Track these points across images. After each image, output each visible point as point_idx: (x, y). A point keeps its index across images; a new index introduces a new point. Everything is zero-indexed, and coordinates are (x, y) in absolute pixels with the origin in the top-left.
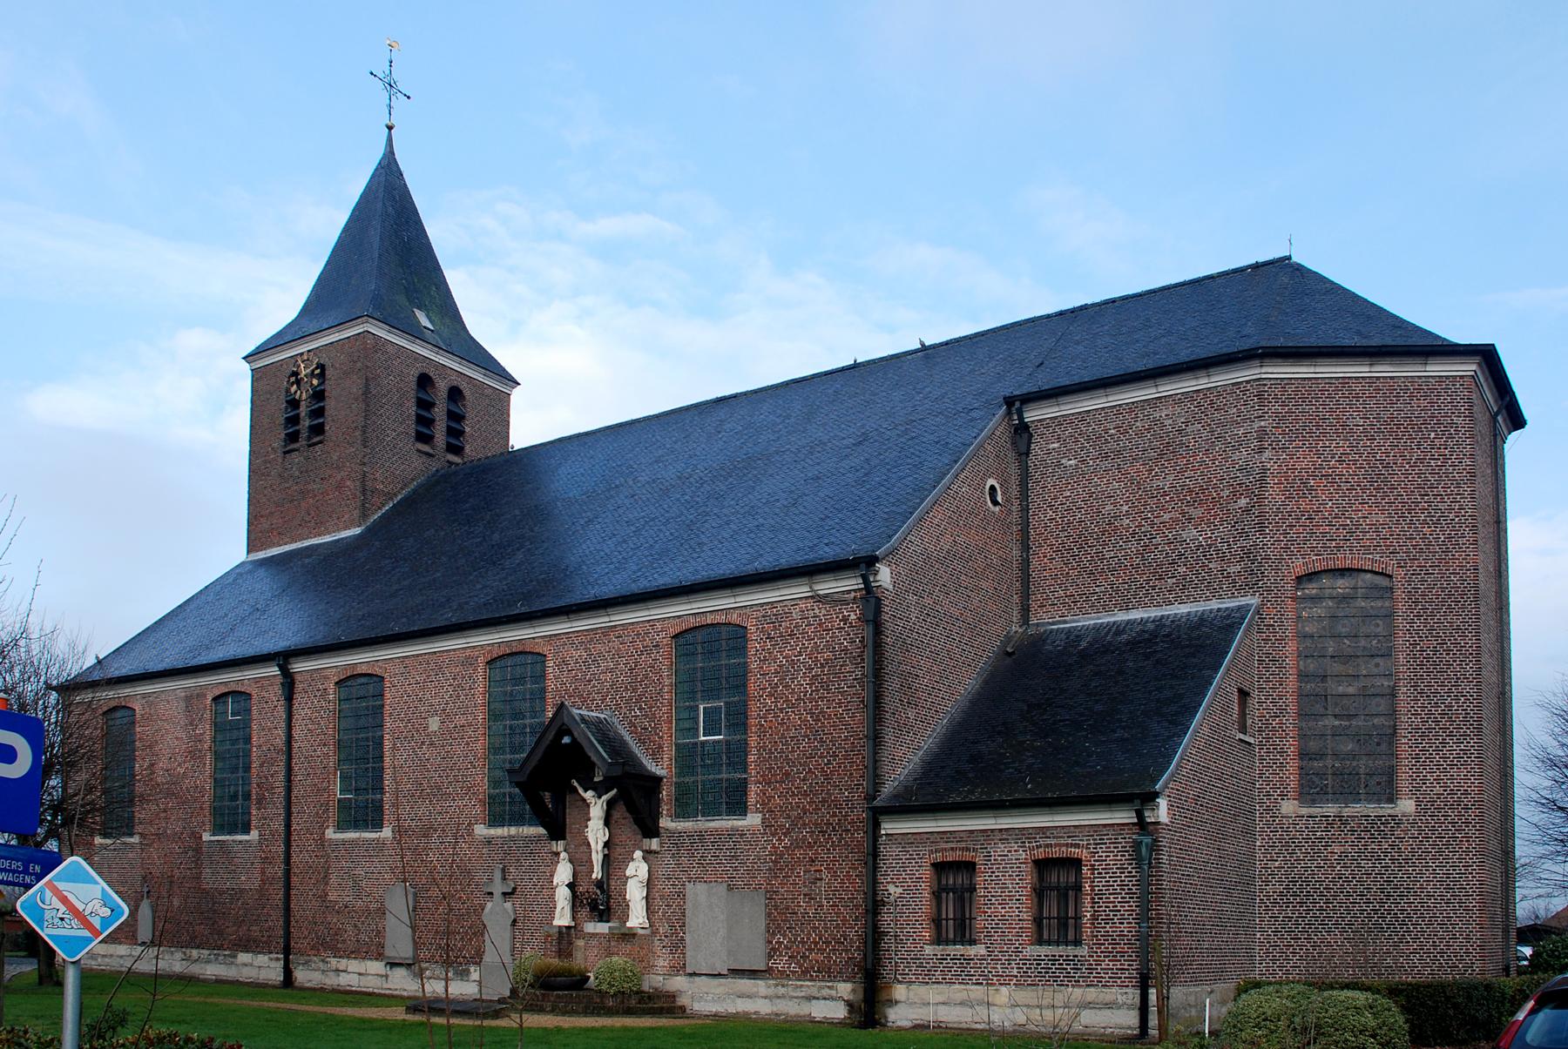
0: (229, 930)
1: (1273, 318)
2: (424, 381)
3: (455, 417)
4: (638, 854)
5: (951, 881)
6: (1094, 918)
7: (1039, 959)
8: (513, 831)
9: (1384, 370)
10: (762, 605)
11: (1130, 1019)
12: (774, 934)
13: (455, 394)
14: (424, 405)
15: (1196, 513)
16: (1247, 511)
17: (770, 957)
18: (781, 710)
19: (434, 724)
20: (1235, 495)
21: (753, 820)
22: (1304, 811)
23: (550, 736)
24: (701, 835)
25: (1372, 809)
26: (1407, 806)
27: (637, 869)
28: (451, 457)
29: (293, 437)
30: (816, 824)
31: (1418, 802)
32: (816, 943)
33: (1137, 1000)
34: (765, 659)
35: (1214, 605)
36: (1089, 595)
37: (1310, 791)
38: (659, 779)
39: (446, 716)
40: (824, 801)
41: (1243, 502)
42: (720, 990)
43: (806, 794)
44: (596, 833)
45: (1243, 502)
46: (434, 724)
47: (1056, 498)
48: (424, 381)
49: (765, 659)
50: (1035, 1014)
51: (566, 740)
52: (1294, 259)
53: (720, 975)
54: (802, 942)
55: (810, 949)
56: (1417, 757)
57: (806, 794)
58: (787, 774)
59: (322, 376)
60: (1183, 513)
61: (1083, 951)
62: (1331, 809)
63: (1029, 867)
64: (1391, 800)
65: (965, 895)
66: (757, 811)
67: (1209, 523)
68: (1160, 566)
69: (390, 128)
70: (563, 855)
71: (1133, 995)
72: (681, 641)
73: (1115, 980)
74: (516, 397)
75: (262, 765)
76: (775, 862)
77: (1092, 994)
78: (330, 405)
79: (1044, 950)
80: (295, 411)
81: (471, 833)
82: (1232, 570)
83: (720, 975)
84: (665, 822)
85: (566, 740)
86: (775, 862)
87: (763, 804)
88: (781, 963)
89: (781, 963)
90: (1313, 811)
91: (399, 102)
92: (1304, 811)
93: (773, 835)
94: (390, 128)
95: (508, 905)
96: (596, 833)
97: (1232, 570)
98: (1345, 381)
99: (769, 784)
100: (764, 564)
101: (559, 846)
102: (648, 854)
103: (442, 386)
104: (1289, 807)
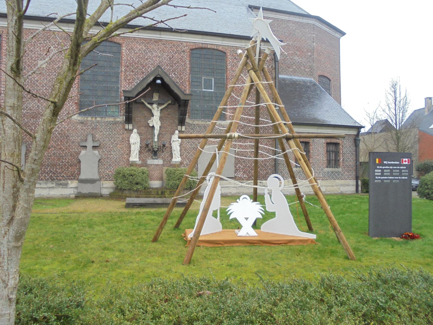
4: (177, 132)
5: (331, 149)
6: (343, 160)
7: (328, 172)
10: (233, 46)
11: (353, 189)
12: (237, 164)
15: (298, 53)
16: (310, 56)
17: (235, 172)
20: (308, 52)
23: (151, 79)
33: (355, 183)
34: (234, 66)
35: (303, 78)
41: (309, 54)
44: (155, 121)
45: (309, 54)
49: (234, 66)
50: (332, 188)
54: (249, 167)
60: (295, 53)
61: (340, 170)
63: (325, 145)
65: (337, 153)
67: (301, 57)
71: (354, 182)
73: (349, 178)
75: (290, 50)
77: (342, 182)
79: (330, 170)
82: (307, 70)
85: (159, 81)
89: (240, 175)
95: (96, 152)
96: (155, 121)
97: (307, 70)
101: (131, 127)
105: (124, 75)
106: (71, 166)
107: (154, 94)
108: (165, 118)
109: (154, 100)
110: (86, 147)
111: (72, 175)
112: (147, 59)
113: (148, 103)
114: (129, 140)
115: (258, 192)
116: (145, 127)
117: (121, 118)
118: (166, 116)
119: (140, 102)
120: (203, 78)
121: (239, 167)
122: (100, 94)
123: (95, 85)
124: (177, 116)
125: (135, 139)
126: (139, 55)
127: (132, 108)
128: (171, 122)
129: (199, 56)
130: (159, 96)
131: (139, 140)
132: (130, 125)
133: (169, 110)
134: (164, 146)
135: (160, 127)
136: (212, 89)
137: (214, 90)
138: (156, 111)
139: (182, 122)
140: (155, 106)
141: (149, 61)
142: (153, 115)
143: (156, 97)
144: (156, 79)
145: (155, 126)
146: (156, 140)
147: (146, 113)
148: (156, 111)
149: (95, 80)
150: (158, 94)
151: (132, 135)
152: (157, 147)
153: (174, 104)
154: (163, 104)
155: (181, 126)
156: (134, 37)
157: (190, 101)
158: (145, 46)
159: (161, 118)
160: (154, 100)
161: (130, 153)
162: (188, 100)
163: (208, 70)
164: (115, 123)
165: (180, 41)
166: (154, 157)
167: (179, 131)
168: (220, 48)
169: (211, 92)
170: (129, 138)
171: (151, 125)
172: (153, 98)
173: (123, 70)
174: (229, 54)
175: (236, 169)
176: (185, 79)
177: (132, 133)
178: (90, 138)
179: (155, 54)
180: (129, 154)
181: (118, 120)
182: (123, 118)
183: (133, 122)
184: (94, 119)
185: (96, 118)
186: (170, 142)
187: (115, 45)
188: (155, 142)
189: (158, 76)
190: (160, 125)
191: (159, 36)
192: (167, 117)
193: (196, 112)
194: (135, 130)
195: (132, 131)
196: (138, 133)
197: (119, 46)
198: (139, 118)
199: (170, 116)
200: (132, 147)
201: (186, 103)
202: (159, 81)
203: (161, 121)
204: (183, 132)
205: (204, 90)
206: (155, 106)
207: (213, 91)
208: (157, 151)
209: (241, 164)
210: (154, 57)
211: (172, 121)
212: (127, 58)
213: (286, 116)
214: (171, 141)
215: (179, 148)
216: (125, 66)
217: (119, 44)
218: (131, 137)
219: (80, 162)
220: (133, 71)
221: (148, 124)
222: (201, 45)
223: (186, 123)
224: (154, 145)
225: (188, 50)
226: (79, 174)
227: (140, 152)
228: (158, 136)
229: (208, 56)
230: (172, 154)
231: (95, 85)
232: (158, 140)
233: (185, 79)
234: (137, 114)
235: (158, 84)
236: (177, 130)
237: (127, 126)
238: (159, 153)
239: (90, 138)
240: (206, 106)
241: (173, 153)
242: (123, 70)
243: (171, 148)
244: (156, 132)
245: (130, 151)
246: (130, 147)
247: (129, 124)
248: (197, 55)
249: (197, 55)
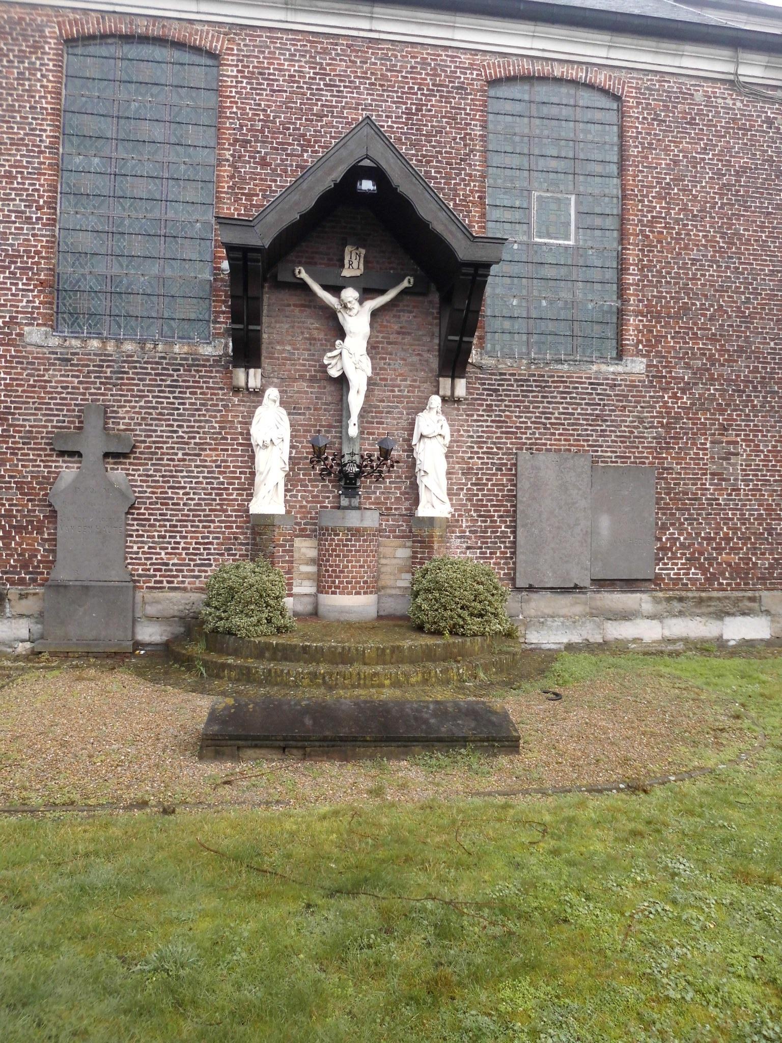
0: (206, 872)
4: (435, 401)
12: (664, 528)
18: (677, 221)
21: (637, 366)
23: (338, 174)
27: (432, 422)
30: (729, 380)
32: (728, 539)
34: (650, 147)
40: (741, 350)
42: (578, 609)
43: (713, 339)
44: (353, 358)
49: (650, 147)
53: (576, 589)
55: (719, 549)
57: (713, 339)
58: (686, 308)
66: (639, 353)
72: (89, 63)
76: (668, 427)
83: (576, 589)
85: (367, 185)
86: (668, 427)
87: (648, 344)
88: (672, 569)
93: (665, 390)
96: (353, 358)
99: (658, 318)
100: (120, 2)
101: (254, 378)
102: (449, 400)
105: (232, 177)
106: (19, 529)
107: (348, 249)
108: (390, 348)
109: (346, 273)
110: (80, 454)
111: (25, 566)
112: (320, 116)
113: (326, 288)
114: (249, 434)
115: (768, 637)
116: (313, 379)
117: (216, 348)
118: (393, 337)
119: (290, 279)
120: (535, 194)
121: (674, 540)
122: (138, 247)
123: (117, 211)
124: (437, 341)
125: (272, 426)
126: (290, 100)
127: (261, 282)
128: (412, 365)
129: (518, 108)
130: (366, 262)
131: (285, 431)
132: (252, 371)
133: (405, 317)
134: (385, 453)
135: (371, 382)
136: (569, 239)
137: (576, 240)
138: (358, 320)
139: (454, 362)
140: (350, 294)
141: (329, 125)
142: (341, 333)
143: (353, 265)
144: (356, 173)
145: (351, 375)
146: (353, 431)
147: (314, 326)
148: (358, 320)
149: (120, 194)
150: (363, 251)
151: (259, 410)
152: (357, 458)
153: (424, 294)
154: (382, 292)
155: (453, 378)
156: (271, 29)
157: (494, 269)
158: (313, 64)
159: (373, 349)
160: (346, 273)
161: (252, 484)
162: (487, 266)
163: (553, 164)
164: (195, 363)
165: (446, 48)
166: (344, 502)
167: (444, 400)
168: (601, 78)
169: (566, 248)
170: (247, 423)
171: (334, 373)
172: (343, 266)
173: (228, 155)
174: (632, 102)
175: (663, 549)
176: (466, 196)
177: (260, 403)
178: (94, 424)
179: (349, 97)
180: (248, 489)
181: (207, 350)
182: (226, 346)
183: (265, 362)
184: (110, 347)
185: (119, 342)
186: (408, 440)
187: (197, 59)
188: (350, 439)
189: (367, 163)
190: (369, 372)
191: (365, 24)
192: (395, 343)
193: (507, 324)
194: (272, 393)
195: (258, 394)
196: (282, 403)
197: (209, 62)
198: (288, 348)
199: (408, 339)
200: (261, 457)
201: (476, 275)
202: (367, 185)
203: (372, 358)
204: (458, 401)
205: (537, 240)
206: (350, 294)
207: (571, 243)
208: (357, 475)
209: (681, 530)
210: (347, 106)
211: (415, 359)
212: (244, 109)
213: (342, 610)
214: (411, 435)
215: (443, 466)
216: (236, 140)
217: (212, 55)
218: (254, 421)
219: (53, 515)
220: (264, 163)
221: (324, 367)
222: (527, 65)
223: (469, 369)
224: (346, 450)
225: (477, 85)
226: (50, 564)
227: (291, 481)
228: (361, 416)
229: (554, 111)
230: (415, 487)
231: (117, 211)
232: (361, 433)
233: (466, 196)
234: (280, 330)
235: (367, 194)
236: (437, 393)
237: (240, 376)
238: (365, 485)
239: (94, 424)
240: (544, 303)
241: (423, 481)
242: (228, 155)
243: (412, 464)
244: (356, 400)
245: (253, 474)
246: (252, 457)
247: (247, 368)
248: (508, 107)
249: (508, 107)
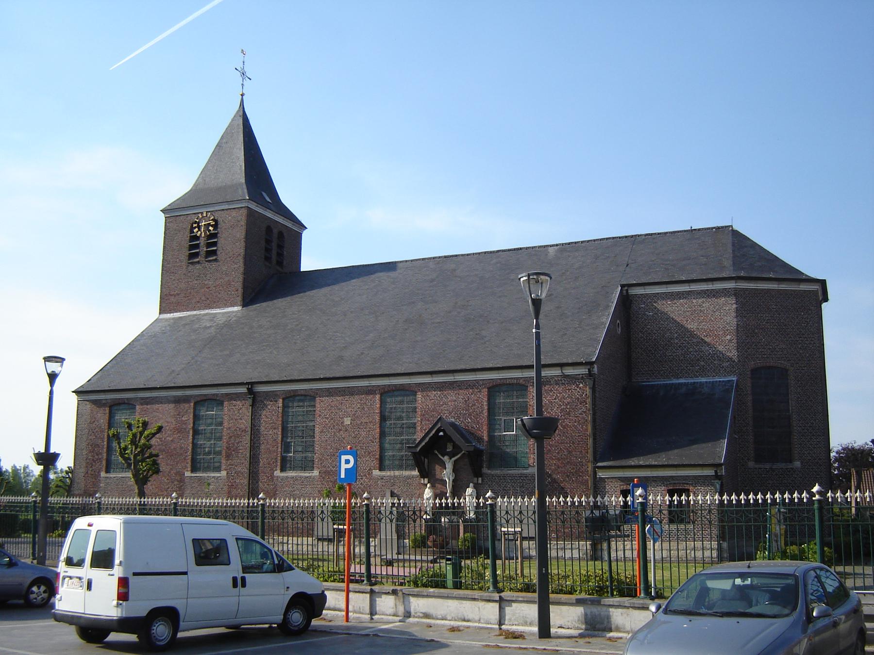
1: (739, 261)
2: (269, 230)
3: (280, 247)
4: (471, 485)
8: (397, 473)
9: (783, 286)
13: (281, 235)
14: (268, 241)
19: (347, 421)
20: (725, 335)
22: (757, 466)
24: (504, 476)
25: (783, 465)
26: (797, 464)
28: (278, 268)
29: (192, 256)
31: (802, 463)
36: (675, 374)
37: (758, 459)
38: (482, 451)
39: (354, 418)
46: (347, 421)
47: (643, 328)
48: (269, 230)
51: (441, 434)
52: (735, 228)
56: (800, 444)
59: (216, 226)
62: (768, 466)
64: (791, 462)
68: (692, 360)
69: (242, 95)
70: (428, 485)
74: (305, 235)
78: (222, 241)
80: (190, 240)
81: (370, 474)
82: (724, 364)
84: (485, 470)
85: (441, 434)
90: (761, 466)
91: (247, 82)
92: (757, 466)
94: (242, 95)
97: (724, 364)
98: (768, 290)
103: (275, 231)
104: (751, 464)
